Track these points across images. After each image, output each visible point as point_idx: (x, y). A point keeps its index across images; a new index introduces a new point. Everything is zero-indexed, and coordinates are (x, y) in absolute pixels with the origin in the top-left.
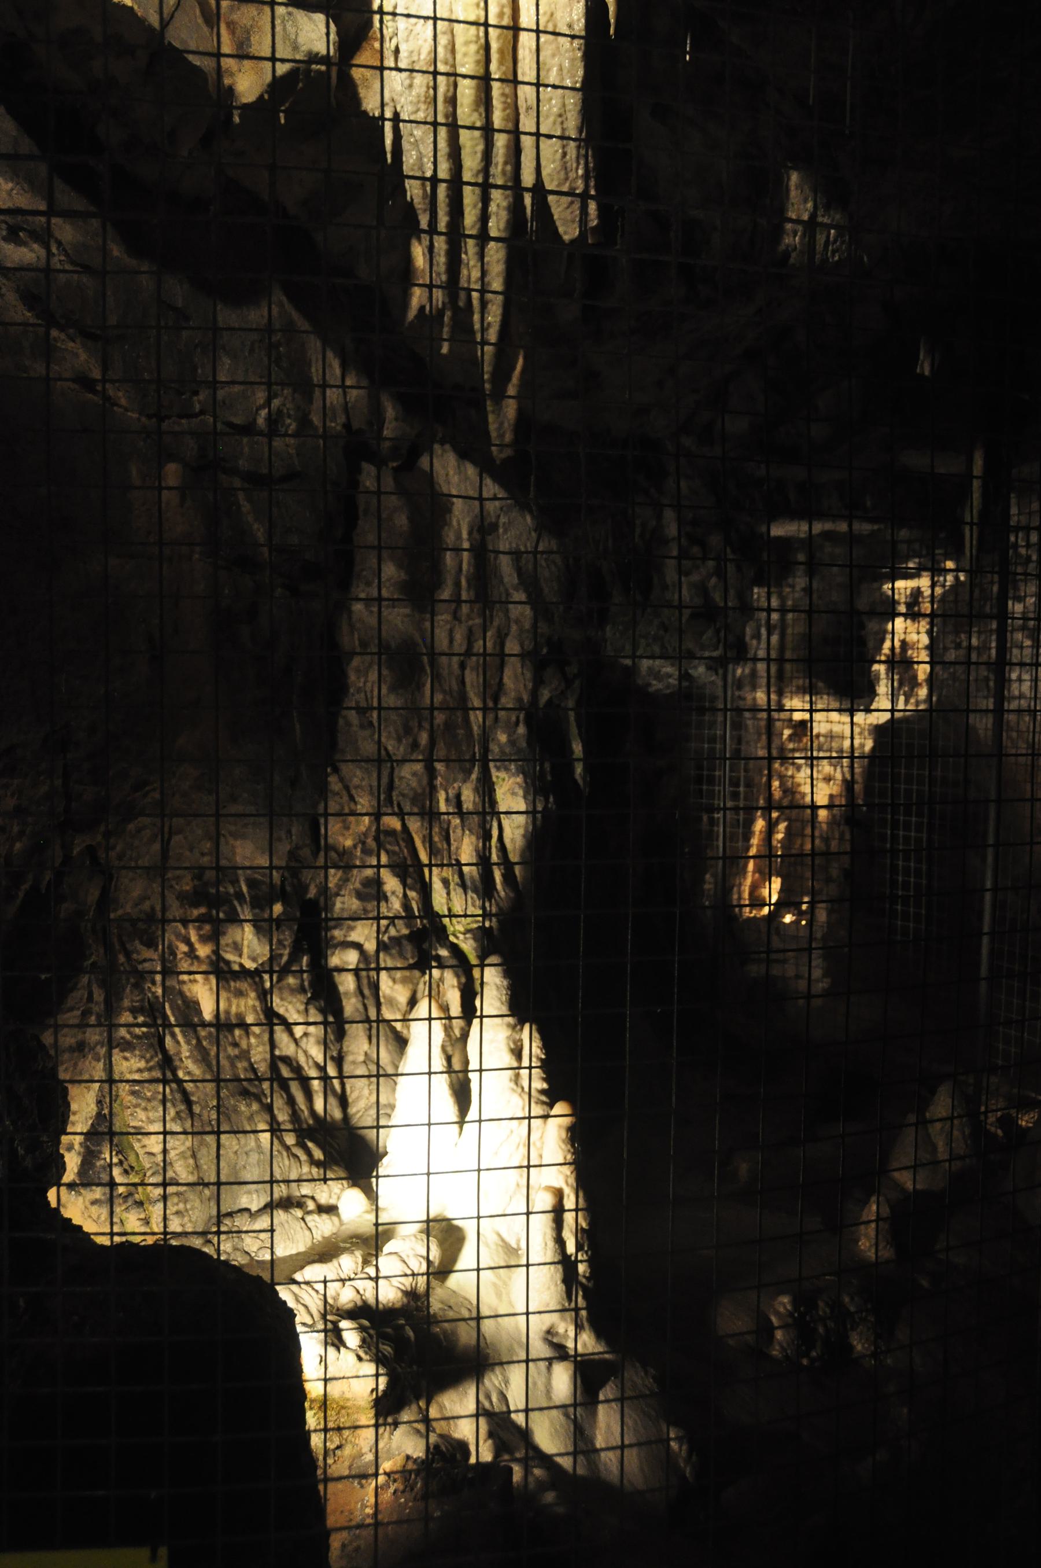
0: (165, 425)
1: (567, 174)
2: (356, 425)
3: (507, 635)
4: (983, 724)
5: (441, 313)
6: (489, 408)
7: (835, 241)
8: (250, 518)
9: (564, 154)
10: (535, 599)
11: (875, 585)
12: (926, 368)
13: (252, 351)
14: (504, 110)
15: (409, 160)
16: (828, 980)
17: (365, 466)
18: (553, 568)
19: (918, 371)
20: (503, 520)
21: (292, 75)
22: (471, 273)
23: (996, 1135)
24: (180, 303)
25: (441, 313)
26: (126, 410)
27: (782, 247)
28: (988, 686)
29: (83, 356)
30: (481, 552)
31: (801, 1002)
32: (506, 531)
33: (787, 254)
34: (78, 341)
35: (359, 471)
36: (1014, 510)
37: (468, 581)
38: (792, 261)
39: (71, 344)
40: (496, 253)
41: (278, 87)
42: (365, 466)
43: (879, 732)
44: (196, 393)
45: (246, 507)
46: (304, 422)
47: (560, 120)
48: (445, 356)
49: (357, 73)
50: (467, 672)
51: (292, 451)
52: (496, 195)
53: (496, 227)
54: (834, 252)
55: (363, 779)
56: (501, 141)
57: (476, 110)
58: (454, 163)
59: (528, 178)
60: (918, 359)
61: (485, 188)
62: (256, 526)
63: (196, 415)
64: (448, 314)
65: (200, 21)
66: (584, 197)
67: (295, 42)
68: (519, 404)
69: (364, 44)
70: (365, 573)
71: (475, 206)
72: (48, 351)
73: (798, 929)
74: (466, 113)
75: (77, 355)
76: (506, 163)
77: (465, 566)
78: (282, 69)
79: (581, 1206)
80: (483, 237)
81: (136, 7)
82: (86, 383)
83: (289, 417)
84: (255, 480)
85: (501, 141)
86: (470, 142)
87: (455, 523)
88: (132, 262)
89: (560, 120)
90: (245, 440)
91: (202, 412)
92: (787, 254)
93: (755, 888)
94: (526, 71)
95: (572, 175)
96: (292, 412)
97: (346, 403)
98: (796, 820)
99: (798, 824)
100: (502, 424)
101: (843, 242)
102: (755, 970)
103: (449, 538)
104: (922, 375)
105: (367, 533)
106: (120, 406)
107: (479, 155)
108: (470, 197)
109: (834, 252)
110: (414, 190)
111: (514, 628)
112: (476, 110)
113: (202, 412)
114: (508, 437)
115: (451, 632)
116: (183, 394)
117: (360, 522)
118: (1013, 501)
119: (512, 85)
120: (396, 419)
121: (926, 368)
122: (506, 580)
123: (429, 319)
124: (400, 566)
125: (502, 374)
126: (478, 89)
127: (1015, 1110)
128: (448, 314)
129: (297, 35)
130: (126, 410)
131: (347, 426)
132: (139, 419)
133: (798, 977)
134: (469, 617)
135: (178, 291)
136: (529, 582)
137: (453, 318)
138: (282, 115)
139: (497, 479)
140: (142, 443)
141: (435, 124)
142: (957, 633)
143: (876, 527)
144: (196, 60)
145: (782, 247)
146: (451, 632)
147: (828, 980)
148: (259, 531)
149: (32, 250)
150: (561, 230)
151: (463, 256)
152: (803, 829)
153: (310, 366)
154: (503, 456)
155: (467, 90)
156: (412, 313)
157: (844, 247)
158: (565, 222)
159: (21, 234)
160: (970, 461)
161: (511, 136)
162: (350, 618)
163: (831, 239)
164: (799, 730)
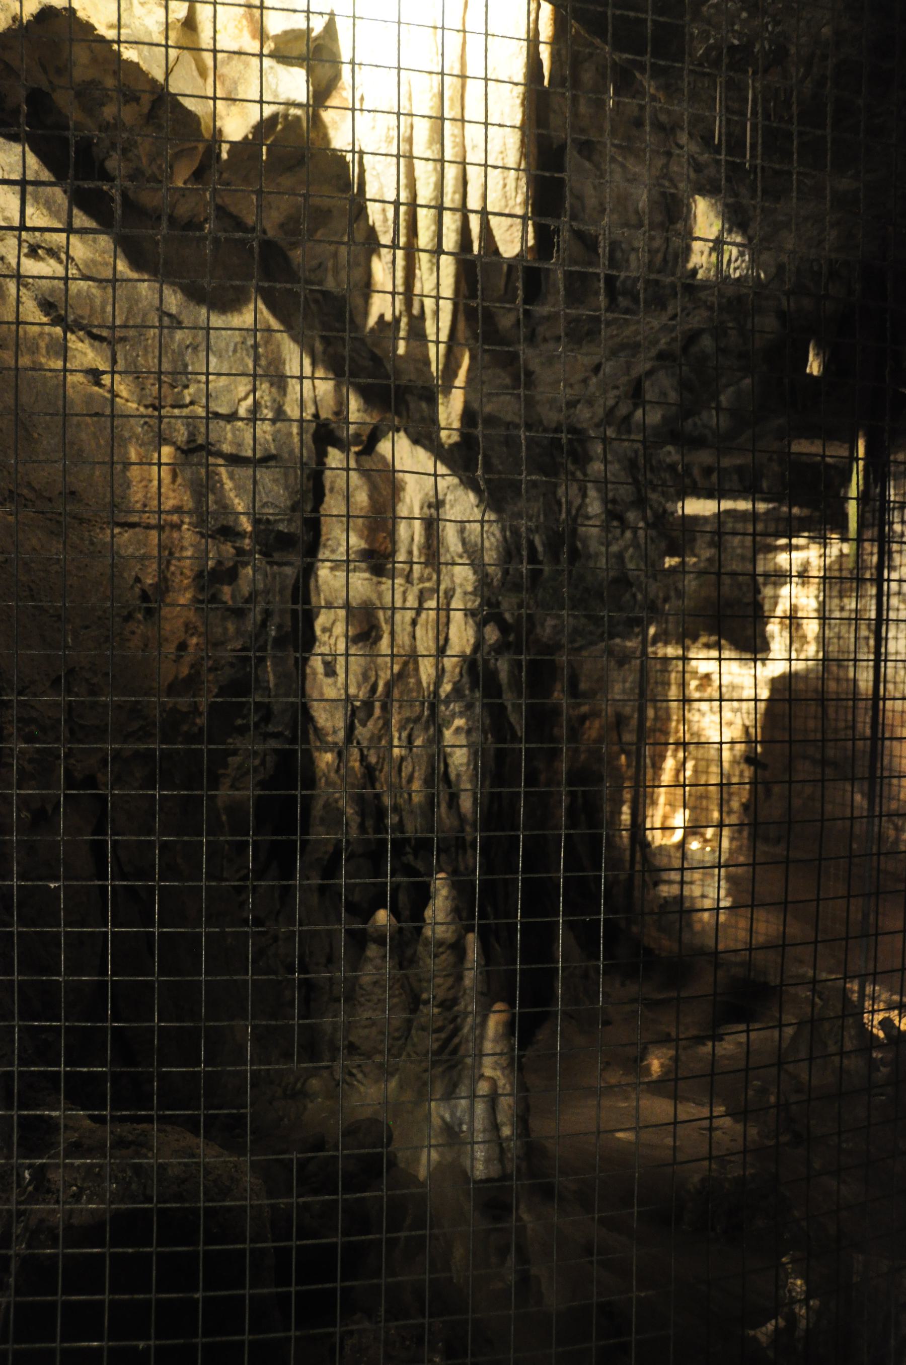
0: (163, 412)
1: (507, 201)
2: (324, 415)
3: (452, 597)
4: (865, 679)
5: (397, 320)
6: (440, 401)
7: (736, 260)
8: (232, 495)
9: (505, 186)
10: (477, 564)
11: (770, 556)
12: (814, 367)
13: (235, 351)
14: (454, 147)
15: (371, 191)
16: (730, 899)
17: (331, 450)
18: (493, 539)
19: (808, 370)
20: (449, 497)
21: (274, 117)
22: (425, 281)
23: (877, 1037)
24: (174, 310)
25: (397, 320)
26: (127, 401)
27: (690, 265)
28: (868, 644)
29: (91, 354)
30: (432, 525)
31: (706, 916)
32: (452, 507)
33: (695, 271)
34: (87, 341)
35: (325, 454)
36: (892, 492)
37: (420, 550)
38: (699, 276)
39: (80, 344)
40: (448, 265)
41: (264, 127)
42: (331, 450)
43: (776, 684)
44: (186, 387)
45: (228, 484)
46: (280, 415)
47: (501, 156)
48: (401, 357)
49: (327, 116)
50: (418, 628)
51: (269, 438)
52: (447, 216)
53: (450, 242)
54: (735, 269)
55: (327, 720)
56: (451, 172)
57: (430, 148)
58: (410, 192)
59: (474, 203)
60: (807, 360)
61: (440, 209)
62: (236, 501)
63: (186, 406)
64: (404, 321)
65: (196, 73)
66: (524, 218)
67: (276, 91)
68: (466, 395)
69: (334, 93)
70: (330, 543)
71: (428, 228)
72: (64, 351)
73: (704, 855)
74: (421, 147)
75: (85, 354)
76: (454, 192)
77: (416, 538)
78: (268, 111)
79: (522, 167)
80: (438, 251)
81: (141, 63)
82: (95, 375)
83: (266, 407)
84: (235, 460)
85: (451, 172)
86: (425, 174)
87: (408, 500)
88: (135, 275)
89: (501, 156)
90: (229, 427)
91: (192, 403)
92: (695, 271)
93: (665, 817)
94: (474, 111)
95: (511, 203)
96: (269, 404)
97: (315, 397)
98: (702, 759)
99: (703, 763)
100: (449, 414)
101: (743, 261)
102: (665, 891)
103: (403, 510)
104: (811, 375)
105: (333, 505)
106: (122, 398)
107: (432, 186)
108: (425, 218)
109: (735, 269)
110: (375, 213)
111: (459, 591)
112: (430, 148)
113: (192, 403)
114: (456, 424)
115: (404, 593)
116: (175, 387)
117: (327, 499)
118: (892, 483)
119: (459, 123)
120: (359, 411)
121: (814, 367)
122: (452, 549)
123: (386, 327)
124: (361, 537)
125: (450, 370)
126: (432, 130)
127: (896, 1012)
128: (404, 321)
129: (277, 85)
130: (127, 401)
131: (316, 416)
132: (137, 409)
133: (703, 896)
134: (421, 580)
135: (173, 300)
136: (473, 554)
137: (409, 324)
138: (264, 149)
139: (445, 462)
140: (140, 429)
141: (398, 156)
142: (841, 597)
143: (771, 506)
144: (189, 104)
145: (690, 265)
146: (404, 593)
147: (730, 899)
148: (240, 505)
149: (48, 265)
150: (502, 249)
151: (417, 271)
152: (708, 767)
153: (284, 363)
154: (451, 441)
155: (422, 131)
156: (372, 321)
157: (744, 265)
158: (505, 242)
159: (40, 251)
160: (853, 447)
161: (461, 166)
162: (317, 581)
163: (733, 258)
164: (705, 681)
